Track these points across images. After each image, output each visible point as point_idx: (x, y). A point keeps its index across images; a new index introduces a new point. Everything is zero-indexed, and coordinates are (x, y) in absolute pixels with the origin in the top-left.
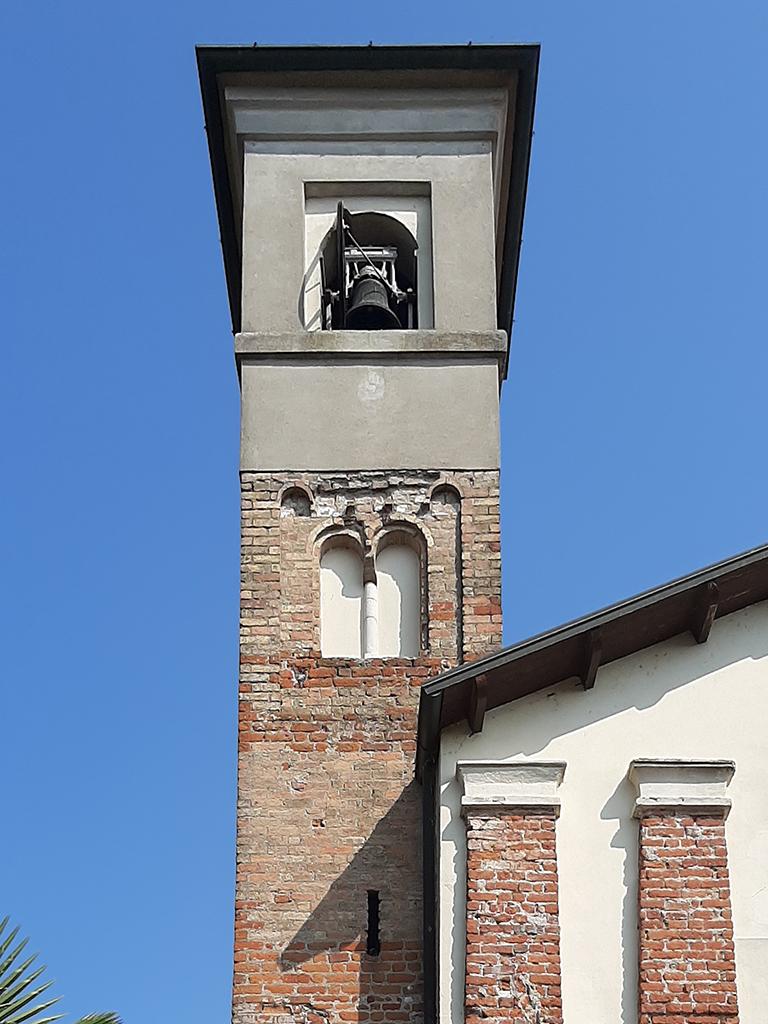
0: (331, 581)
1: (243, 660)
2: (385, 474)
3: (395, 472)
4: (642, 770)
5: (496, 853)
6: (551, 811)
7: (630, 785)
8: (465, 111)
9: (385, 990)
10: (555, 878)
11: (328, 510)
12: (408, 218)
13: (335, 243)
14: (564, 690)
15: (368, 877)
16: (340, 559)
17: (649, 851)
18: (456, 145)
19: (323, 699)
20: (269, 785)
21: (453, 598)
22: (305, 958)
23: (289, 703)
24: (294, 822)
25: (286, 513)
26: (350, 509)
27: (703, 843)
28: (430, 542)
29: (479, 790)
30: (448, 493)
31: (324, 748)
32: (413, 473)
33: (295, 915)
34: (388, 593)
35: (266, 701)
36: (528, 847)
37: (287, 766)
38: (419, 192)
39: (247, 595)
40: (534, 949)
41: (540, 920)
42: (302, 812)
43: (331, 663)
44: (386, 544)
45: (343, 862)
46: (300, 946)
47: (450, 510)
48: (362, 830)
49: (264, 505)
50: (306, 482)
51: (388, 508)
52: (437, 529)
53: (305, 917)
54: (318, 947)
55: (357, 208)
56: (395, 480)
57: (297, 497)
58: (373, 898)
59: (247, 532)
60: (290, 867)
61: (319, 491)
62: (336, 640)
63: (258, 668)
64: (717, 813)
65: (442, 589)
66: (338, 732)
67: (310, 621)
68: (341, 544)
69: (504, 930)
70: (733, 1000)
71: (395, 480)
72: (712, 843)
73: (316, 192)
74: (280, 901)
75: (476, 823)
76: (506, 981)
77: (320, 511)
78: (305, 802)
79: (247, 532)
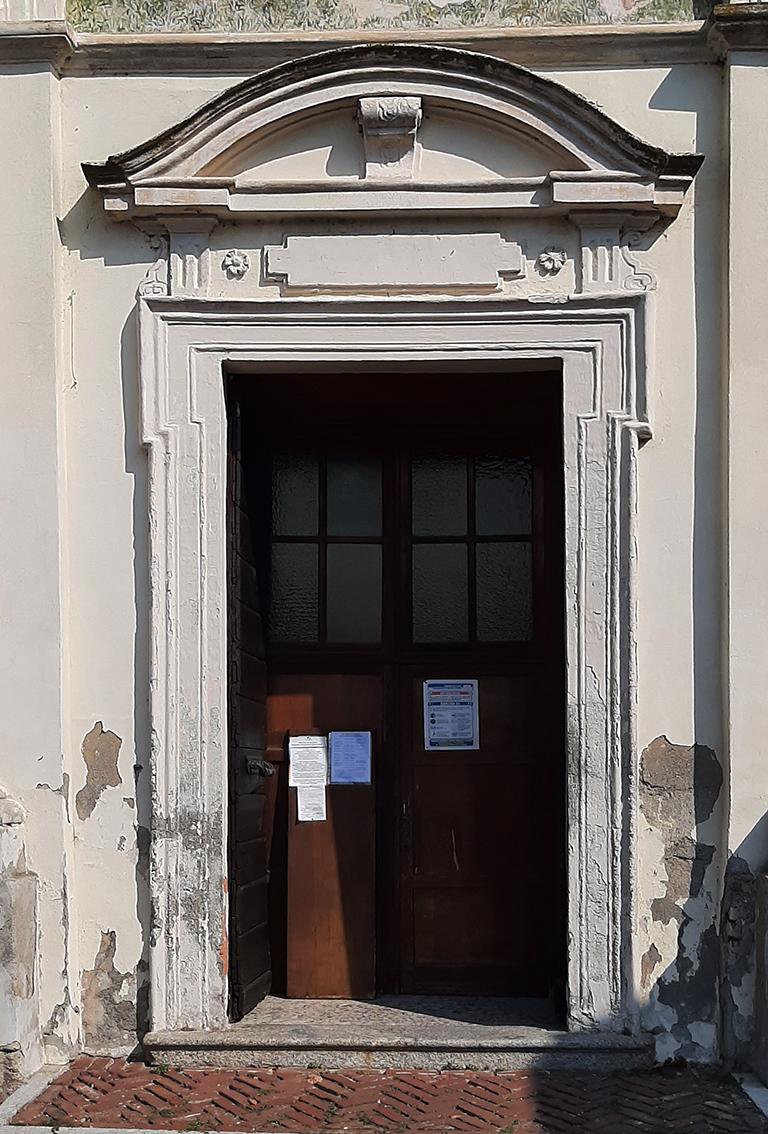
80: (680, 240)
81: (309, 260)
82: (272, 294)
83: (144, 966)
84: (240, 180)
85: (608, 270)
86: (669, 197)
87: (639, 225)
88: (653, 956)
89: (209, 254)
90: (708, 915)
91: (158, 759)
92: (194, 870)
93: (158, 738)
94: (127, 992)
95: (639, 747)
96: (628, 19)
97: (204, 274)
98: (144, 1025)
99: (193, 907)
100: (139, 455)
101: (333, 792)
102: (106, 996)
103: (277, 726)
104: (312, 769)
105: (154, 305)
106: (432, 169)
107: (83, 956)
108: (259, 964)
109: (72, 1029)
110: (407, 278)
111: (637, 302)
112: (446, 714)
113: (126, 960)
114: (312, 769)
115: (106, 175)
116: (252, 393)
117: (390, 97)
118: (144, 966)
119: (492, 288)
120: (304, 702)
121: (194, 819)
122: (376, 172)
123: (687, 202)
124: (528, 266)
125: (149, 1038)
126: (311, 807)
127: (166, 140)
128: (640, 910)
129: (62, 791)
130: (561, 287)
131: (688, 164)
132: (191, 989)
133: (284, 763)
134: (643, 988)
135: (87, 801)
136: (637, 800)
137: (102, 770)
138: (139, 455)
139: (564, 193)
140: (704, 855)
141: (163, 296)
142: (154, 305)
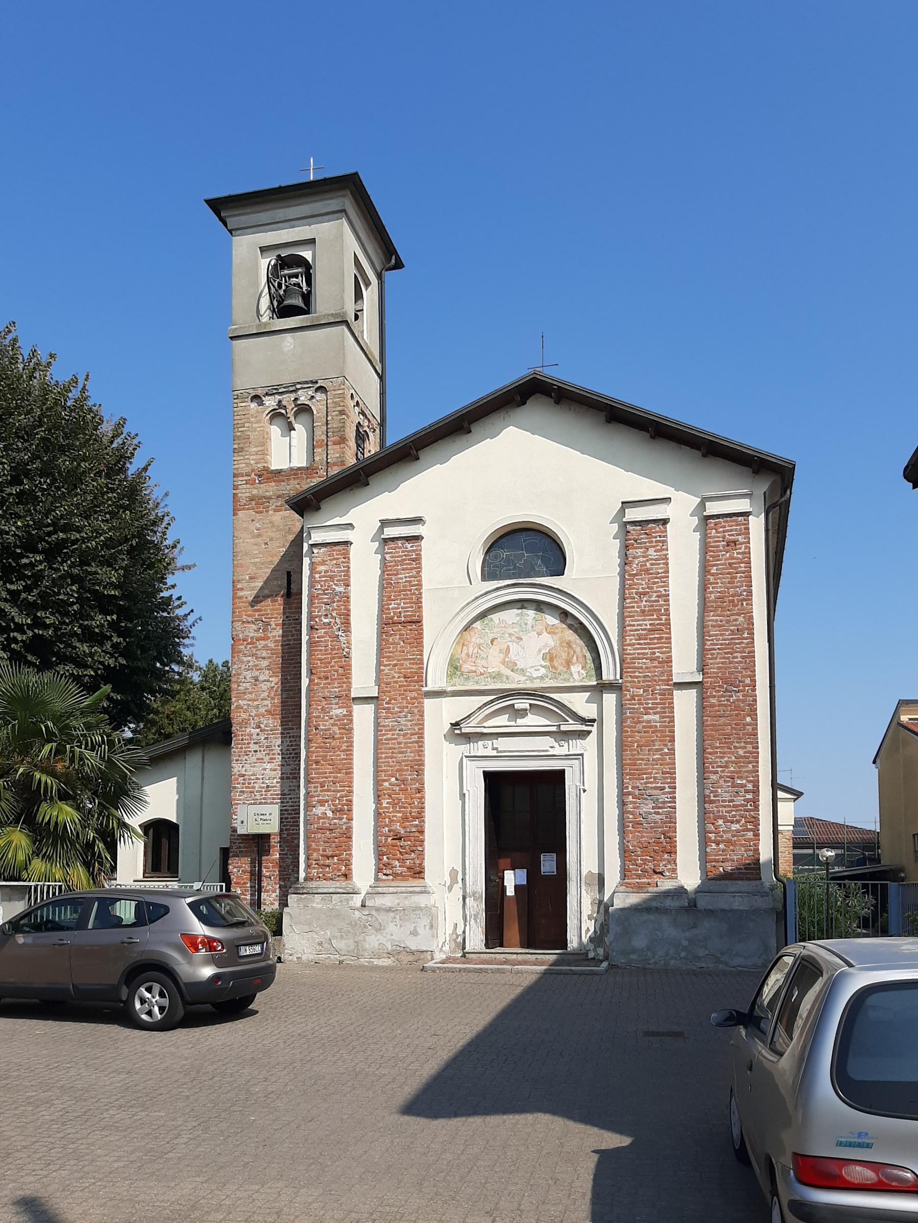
0: (275, 431)
1: (235, 476)
2: (294, 384)
3: (299, 383)
4: (385, 523)
5: (323, 563)
6: (347, 543)
7: (381, 529)
8: (328, 202)
9: (293, 613)
10: (348, 571)
11: (270, 402)
12: (307, 255)
13: (274, 272)
14: (357, 487)
15: (286, 566)
16: (279, 420)
17: (388, 557)
18: (326, 217)
19: (270, 489)
20: (246, 529)
21: (324, 437)
22: (261, 601)
23: (255, 492)
24: (256, 545)
25: (253, 405)
26: (280, 401)
27: (410, 551)
28: (315, 412)
29: (317, 537)
30: (321, 389)
31: (267, 511)
32: (306, 382)
33: (257, 584)
34: (300, 433)
35: (245, 492)
36: (337, 559)
37: (253, 520)
38: (312, 241)
39: (236, 446)
40: (338, 601)
41: (341, 589)
42: (259, 540)
43: (272, 472)
44: (296, 415)
45: (276, 560)
46: (259, 597)
47: (323, 396)
48: (284, 546)
49: (243, 404)
50: (260, 392)
51: (296, 399)
52: (318, 405)
53: (260, 584)
54: (266, 597)
55: (284, 253)
56: (299, 386)
57: (256, 398)
58: (289, 574)
59: (236, 418)
60: (255, 564)
61: (267, 394)
62: (277, 462)
63: (241, 478)
64: (417, 538)
65: (320, 435)
66: (274, 504)
67: (264, 453)
68: (276, 415)
69: (326, 594)
70: (421, 616)
71: (299, 386)
72: (414, 551)
73: (264, 250)
74: (251, 578)
75: (315, 551)
76: (326, 615)
77: (267, 403)
78: (259, 535)
79: (236, 418)
80: (593, 737)
81: (504, 744)
82: (494, 753)
83: (464, 932)
84: (485, 724)
85: (576, 746)
86: (589, 728)
87: (583, 735)
88: (588, 930)
89: (480, 742)
90: (601, 919)
91: (467, 877)
92: (478, 907)
93: (467, 871)
94: (460, 939)
95: (584, 873)
96: (581, 681)
97: (480, 748)
98: (464, 948)
99: (476, 917)
100: (463, 796)
101: (517, 887)
102: (455, 941)
103: (501, 868)
104: (511, 880)
105: (466, 757)
106: (533, 721)
107: (449, 930)
108: (495, 935)
109: (446, 948)
110: (526, 750)
111: (582, 755)
112: (547, 864)
113: (460, 931)
114: (511, 880)
115: (456, 725)
116: (491, 778)
117: (522, 704)
118: (464, 932)
119: (547, 751)
120: (508, 861)
121: (476, 892)
122: (520, 721)
123: (594, 729)
124: (556, 745)
125: (467, 950)
126: (510, 892)
127: (469, 716)
128: (585, 917)
129: (445, 885)
130: (564, 751)
131: (594, 721)
132: (476, 938)
133: (502, 879)
134: (585, 940)
135: (450, 889)
136: (583, 888)
137: (454, 880)
138: (463, 796)
139: (563, 728)
140: (601, 902)
141: (468, 754)
142: (466, 757)
